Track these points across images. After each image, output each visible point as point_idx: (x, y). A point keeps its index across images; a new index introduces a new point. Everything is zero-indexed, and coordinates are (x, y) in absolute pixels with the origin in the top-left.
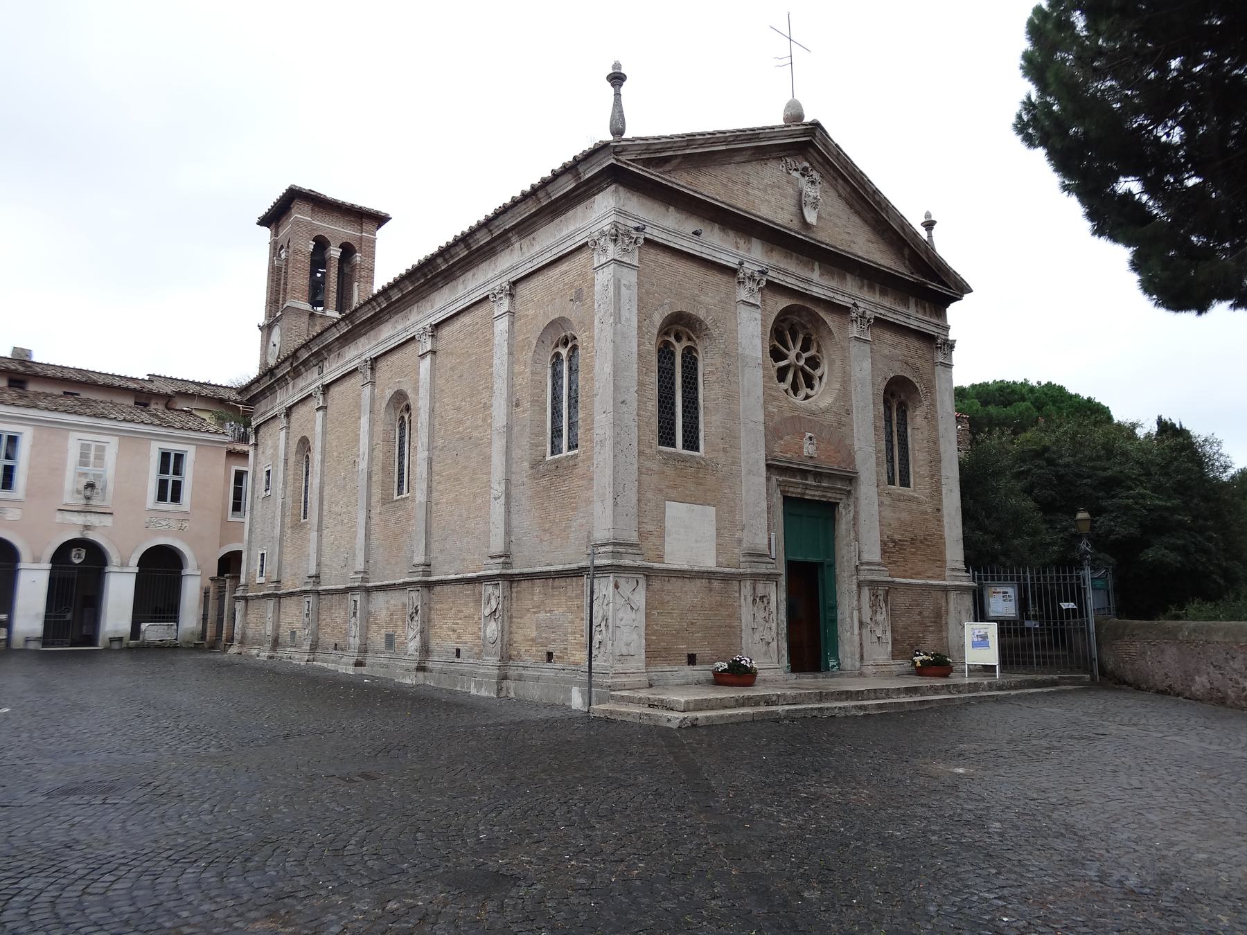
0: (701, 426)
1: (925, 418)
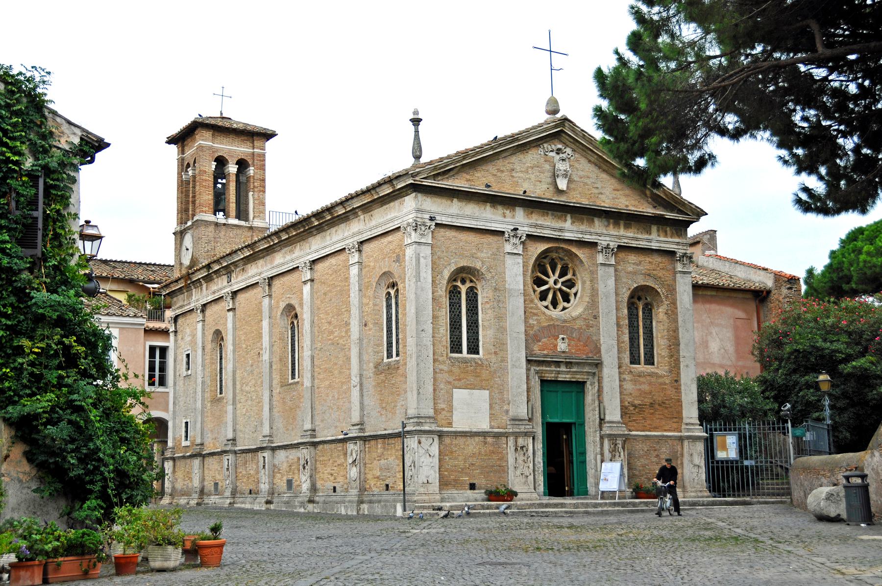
0: (480, 338)
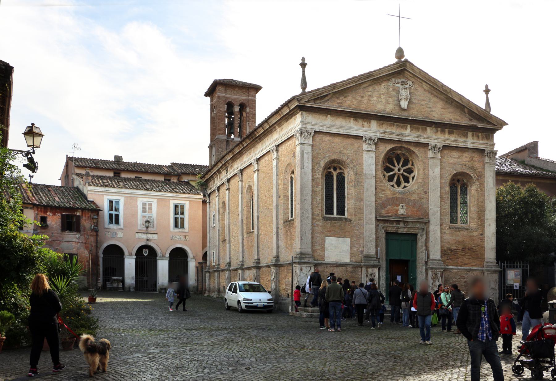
0: (346, 205)
1: (476, 191)
